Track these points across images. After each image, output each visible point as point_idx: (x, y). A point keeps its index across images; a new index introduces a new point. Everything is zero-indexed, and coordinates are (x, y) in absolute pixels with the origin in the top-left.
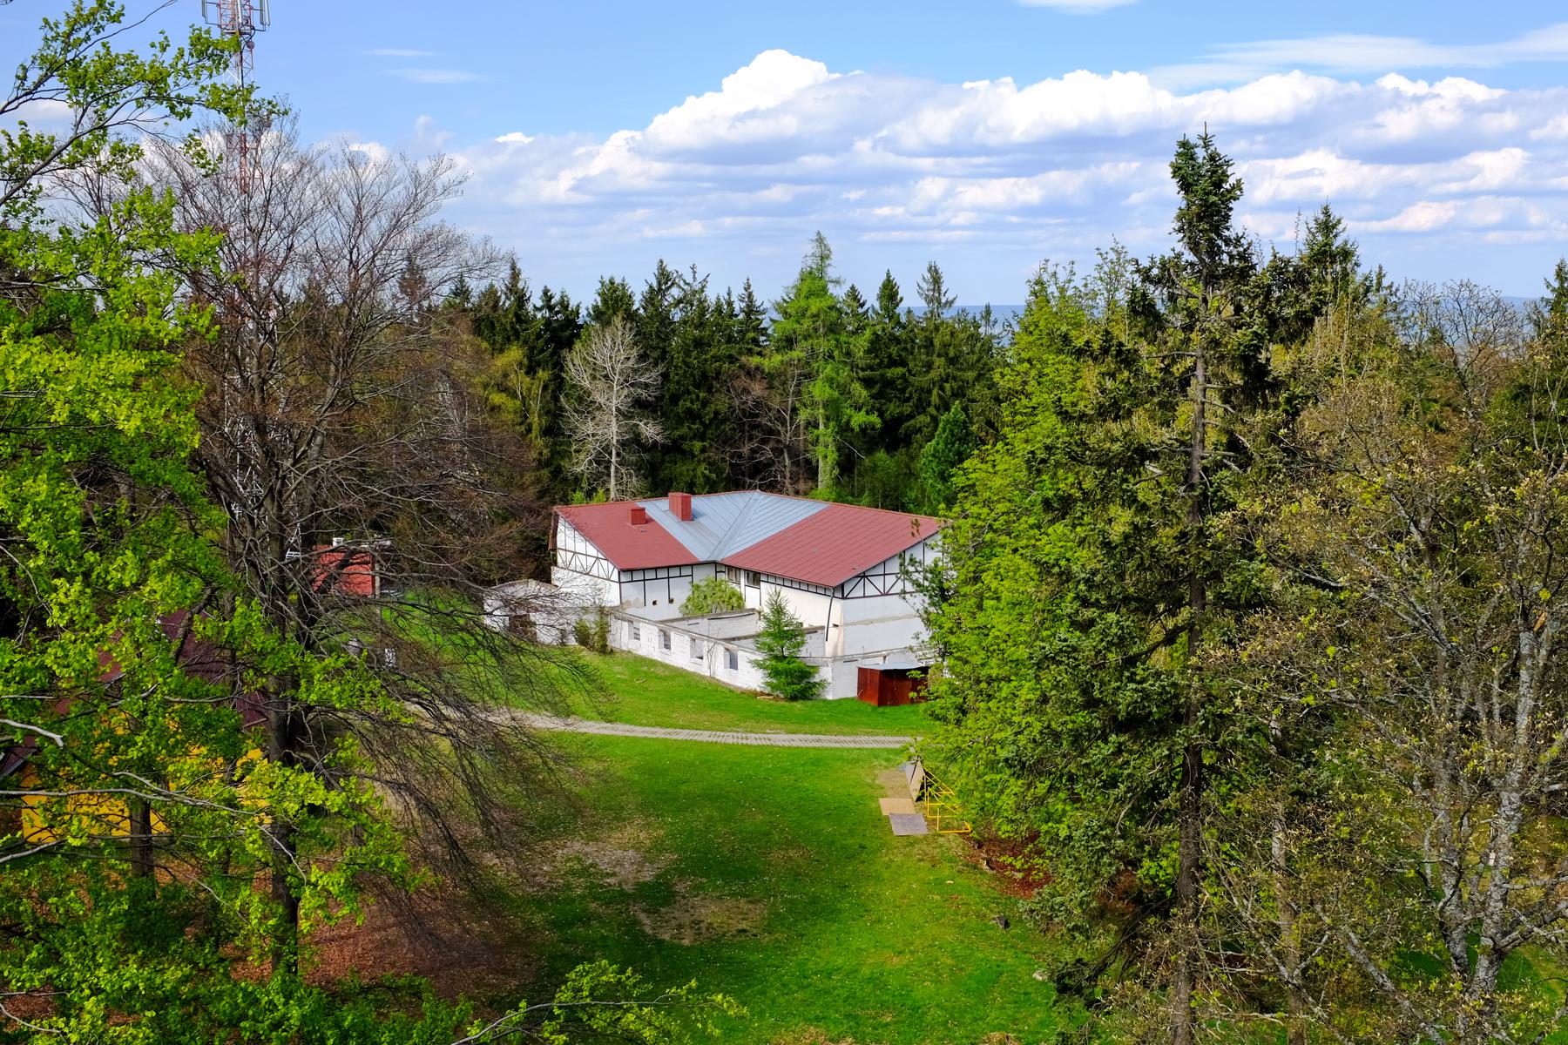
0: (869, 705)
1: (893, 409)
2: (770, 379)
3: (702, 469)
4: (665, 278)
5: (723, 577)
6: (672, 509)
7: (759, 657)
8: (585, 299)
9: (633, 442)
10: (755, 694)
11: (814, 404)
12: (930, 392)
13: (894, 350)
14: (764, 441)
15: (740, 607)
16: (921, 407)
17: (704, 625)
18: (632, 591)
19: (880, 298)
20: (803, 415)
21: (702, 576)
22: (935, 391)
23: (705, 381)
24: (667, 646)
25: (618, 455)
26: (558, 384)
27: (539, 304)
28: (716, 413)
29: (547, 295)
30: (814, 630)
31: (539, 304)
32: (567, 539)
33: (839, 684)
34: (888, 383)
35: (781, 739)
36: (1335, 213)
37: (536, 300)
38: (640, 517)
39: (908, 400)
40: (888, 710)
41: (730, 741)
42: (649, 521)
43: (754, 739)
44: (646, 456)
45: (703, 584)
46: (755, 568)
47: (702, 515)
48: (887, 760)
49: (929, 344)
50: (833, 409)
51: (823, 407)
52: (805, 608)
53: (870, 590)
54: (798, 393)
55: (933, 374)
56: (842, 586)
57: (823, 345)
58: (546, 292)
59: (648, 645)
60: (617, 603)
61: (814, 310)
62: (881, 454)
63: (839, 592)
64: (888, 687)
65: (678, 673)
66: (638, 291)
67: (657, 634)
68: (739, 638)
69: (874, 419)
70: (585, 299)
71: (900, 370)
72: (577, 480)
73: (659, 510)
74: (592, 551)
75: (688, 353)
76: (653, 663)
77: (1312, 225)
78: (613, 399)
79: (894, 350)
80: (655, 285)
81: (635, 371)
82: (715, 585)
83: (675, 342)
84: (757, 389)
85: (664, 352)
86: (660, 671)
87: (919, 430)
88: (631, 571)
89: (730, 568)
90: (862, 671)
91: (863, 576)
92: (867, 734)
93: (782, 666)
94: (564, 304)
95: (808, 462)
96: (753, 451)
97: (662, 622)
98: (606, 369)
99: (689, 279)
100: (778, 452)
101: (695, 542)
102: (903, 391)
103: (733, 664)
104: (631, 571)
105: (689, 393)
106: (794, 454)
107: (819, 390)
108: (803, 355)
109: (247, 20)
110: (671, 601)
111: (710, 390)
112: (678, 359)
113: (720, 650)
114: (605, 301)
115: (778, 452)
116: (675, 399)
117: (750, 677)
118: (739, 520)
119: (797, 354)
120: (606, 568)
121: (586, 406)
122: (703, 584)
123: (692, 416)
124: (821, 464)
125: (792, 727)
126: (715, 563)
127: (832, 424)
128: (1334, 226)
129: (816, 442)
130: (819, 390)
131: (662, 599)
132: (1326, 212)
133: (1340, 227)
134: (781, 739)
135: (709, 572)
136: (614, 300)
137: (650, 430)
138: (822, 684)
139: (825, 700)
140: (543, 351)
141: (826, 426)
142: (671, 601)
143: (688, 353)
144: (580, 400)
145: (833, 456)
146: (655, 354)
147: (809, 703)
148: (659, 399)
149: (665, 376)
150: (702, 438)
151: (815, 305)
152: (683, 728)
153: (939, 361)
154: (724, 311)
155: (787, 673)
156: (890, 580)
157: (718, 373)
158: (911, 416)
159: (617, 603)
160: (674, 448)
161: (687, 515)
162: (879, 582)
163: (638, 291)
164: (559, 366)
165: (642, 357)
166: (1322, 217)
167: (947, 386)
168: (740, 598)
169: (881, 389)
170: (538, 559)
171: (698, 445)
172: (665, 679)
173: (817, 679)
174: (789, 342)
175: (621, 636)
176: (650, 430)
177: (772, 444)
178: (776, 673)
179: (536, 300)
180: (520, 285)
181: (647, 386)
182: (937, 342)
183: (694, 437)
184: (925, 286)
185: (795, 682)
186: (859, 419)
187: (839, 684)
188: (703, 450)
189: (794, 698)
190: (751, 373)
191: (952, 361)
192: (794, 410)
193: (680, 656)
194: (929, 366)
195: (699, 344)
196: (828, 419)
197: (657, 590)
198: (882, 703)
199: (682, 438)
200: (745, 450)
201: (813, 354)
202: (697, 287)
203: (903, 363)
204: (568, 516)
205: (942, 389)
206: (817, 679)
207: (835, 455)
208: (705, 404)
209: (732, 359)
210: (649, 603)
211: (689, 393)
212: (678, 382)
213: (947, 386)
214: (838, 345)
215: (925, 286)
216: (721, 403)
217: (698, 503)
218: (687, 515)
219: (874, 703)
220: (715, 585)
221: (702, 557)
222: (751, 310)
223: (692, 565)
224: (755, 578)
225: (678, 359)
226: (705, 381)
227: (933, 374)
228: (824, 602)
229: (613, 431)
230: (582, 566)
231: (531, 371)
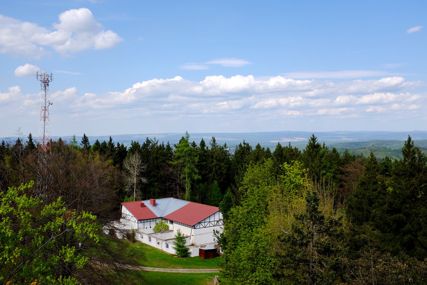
0: (202, 258)
1: (203, 172)
2: (174, 167)
3: (157, 190)
4: (148, 141)
5: (164, 221)
6: (151, 203)
7: (175, 246)
8: (128, 146)
9: (140, 183)
10: (173, 255)
11: (185, 174)
12: (213, 168)
13: (204, 158)
14: (173, 182)
15: (168, 229)
16: (211, 172)
17: (159, 235)
18: (141, 225)
19: (200, 145)
20: (182, 176)
21: (158, 221)
22: (214, 168)
23: (158, 167)
24: (150, 241)
25: (136, 186)
26: (121, 168)
27: (116, 146)
28: (161, 175)
29: (118, 144)
30: (187, 237)
31: (116, 146)
32: (124, 210)
33: (194, 253)
34: (203, 166)
35: (182, 271)
36: (315, 136)
37: (116, 146)
38: (143, 205)
39: (207, 170)
40: (207, 260)
41: (168, 271)
42: (145, 206)
43: (174, 271)
44: (143, 186)
45: (159, 223)
46: (172, 220)
47: (158, 204)
48: (209, 279)
49: (212, 157)
50: (190, 175)
51: (187, 173)
52: (185, 231)
53: (201, 226)
54: (181, 170)
55: (213, 164)
56: (194, 226)
57: (187, 159)
58: (118, 143)
59: (145, 240)
60: (137, 228)
61: (185, 150)
62: (201, 184)
63: (194, 227)
64: (207, 255)
65: (153, 249)
66: (141, 144)
67: (148, 237)
68: (169, 240)
69: (200, 177)
70: (128, 146)
71: (205, 163)
72: (126, 192)
73: (147, 203)
74: (131, 214)
75: (154, 160)
76: (146, 245)
77: (310, 139)
78: (135, 172)
79: (204, 158)
80: (146, 143)
81: (141, 165)
82: (162, 223)
83: (151, 158)
84: (171, 170)
85: (148, 160)
86: (148, 248)
87: (210, 178)
88: (141, 220)
89: (165, 219)
90: (200, 250)
91: (200, 223)
92: (203, 268)
93: (180, 249)
94: (123, 146)
95: (183, 188)
96: (170, 185)
97: (149, 234)
98: (134, 163)
99: (154, 141)
100: (176, 185)
101: (157, 212)
102: (206, 168)
103: (167, 247)
104: (141, 220)
105: (154, 170)
106: (180, 185)
107: (186, 170)
108: (182, 161)
109: (48, 79)
110: (151, 227)
111: (159, 170)
112: (151, 161)
113: (164, 243)
114: (133, 147)
115: (176, 185)
116: (150, 172)
117: (172, 250)
118: (168, 206)
119: (181, 161)
120: (134, 219)
121: (128, 173)
122: (159, 223)
123: (155, 176)
124: (186, 188)
125: (184, 266)
126: (161, 218)
127: (189, 178)
128: (315, 139)
129: (185, 183)
130: (186, 170)
131: (149, 227)
132: (313, 136)
133: (317, 139)
134: (182, 271)
135: (160, 220)
136: (135, 146)
137: (144, 180)
138: (190, 253)
139: (191, 257)
140: (117, 159)
141: (188, 179)
142: (151, 227)
143: (154, 160)
144: (127, 172)
145: (189, 187)
146: (146, 160)
147: (187, 258)
148: (146, 172)
149: (148, 166)
150: (157, 182)
151: (186, 149)
152: (156, 267)
153: (215, 161)
154: (161, 147)
155: (182, 250)
156: (206, 224)
157: (161, 165)
158: (208, 174)
159: (137, 228)
160: (150, 184)
161: (155, 205)
162: (203, 224)
163: (141, 144)
164: (122, 165)
165: (143, 162)
166: (312, 137)
167: (217, 167)
168: (168, 227)
169: (200, 167)
170: (118, 216)
171: (156, 183)
172: (150, 250)
173: (189, 252)
174: (179, 158)
175: (138, 237)
176: (144, 180)
177: (174, 183)
178: (178, 250)
179: (116, 146)
180: (112, 142)
181: (143, 169)
182: (214, 156)
183: (155, 182)
184: (211, 142)
185: (183, 252)
186: (196, 177)
187: (194, 253)
188: (157, 185)
189: (183, 257)
190: (170, 166)
191: (218, 161)
192: (180, 175)
193: (153, 244)
194: (212, 162)
195: (157, 158)
196: (188, 177)
197: (147, 225)
198: (205, 258)
199: (152, 182)
200: (167, 185)
201: (185, 161)
202: (156, 143)
203: (206, 161)
204: (124, 205)
205: (216, 167)
206: (189, 252)
207: (190, 186)
208: (158, 173)
209: (164, 161)
210: (145, 228)
211: (154, 170)
212: (151, 168)
213: (217, 167)
214: (191, 159)
215: (211, 142)
216: (162, 173)
217: (157, 201)
218: (155, 205)
219: (203, 258)
220: (162, 223)
221: (159, 216)
222: (168, 146)
223: (156, 218)
224: (172, 222)
225: (151, 161)
226: (158, 167)
227: (213, 164)
228: (190, 229)
229: (135, 180)
230: (129, 220)
231: (114, 165)
